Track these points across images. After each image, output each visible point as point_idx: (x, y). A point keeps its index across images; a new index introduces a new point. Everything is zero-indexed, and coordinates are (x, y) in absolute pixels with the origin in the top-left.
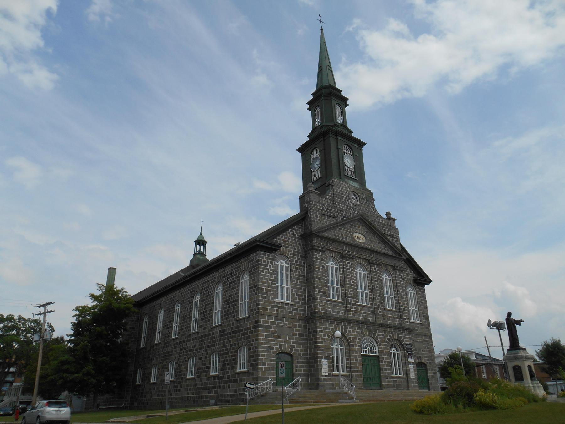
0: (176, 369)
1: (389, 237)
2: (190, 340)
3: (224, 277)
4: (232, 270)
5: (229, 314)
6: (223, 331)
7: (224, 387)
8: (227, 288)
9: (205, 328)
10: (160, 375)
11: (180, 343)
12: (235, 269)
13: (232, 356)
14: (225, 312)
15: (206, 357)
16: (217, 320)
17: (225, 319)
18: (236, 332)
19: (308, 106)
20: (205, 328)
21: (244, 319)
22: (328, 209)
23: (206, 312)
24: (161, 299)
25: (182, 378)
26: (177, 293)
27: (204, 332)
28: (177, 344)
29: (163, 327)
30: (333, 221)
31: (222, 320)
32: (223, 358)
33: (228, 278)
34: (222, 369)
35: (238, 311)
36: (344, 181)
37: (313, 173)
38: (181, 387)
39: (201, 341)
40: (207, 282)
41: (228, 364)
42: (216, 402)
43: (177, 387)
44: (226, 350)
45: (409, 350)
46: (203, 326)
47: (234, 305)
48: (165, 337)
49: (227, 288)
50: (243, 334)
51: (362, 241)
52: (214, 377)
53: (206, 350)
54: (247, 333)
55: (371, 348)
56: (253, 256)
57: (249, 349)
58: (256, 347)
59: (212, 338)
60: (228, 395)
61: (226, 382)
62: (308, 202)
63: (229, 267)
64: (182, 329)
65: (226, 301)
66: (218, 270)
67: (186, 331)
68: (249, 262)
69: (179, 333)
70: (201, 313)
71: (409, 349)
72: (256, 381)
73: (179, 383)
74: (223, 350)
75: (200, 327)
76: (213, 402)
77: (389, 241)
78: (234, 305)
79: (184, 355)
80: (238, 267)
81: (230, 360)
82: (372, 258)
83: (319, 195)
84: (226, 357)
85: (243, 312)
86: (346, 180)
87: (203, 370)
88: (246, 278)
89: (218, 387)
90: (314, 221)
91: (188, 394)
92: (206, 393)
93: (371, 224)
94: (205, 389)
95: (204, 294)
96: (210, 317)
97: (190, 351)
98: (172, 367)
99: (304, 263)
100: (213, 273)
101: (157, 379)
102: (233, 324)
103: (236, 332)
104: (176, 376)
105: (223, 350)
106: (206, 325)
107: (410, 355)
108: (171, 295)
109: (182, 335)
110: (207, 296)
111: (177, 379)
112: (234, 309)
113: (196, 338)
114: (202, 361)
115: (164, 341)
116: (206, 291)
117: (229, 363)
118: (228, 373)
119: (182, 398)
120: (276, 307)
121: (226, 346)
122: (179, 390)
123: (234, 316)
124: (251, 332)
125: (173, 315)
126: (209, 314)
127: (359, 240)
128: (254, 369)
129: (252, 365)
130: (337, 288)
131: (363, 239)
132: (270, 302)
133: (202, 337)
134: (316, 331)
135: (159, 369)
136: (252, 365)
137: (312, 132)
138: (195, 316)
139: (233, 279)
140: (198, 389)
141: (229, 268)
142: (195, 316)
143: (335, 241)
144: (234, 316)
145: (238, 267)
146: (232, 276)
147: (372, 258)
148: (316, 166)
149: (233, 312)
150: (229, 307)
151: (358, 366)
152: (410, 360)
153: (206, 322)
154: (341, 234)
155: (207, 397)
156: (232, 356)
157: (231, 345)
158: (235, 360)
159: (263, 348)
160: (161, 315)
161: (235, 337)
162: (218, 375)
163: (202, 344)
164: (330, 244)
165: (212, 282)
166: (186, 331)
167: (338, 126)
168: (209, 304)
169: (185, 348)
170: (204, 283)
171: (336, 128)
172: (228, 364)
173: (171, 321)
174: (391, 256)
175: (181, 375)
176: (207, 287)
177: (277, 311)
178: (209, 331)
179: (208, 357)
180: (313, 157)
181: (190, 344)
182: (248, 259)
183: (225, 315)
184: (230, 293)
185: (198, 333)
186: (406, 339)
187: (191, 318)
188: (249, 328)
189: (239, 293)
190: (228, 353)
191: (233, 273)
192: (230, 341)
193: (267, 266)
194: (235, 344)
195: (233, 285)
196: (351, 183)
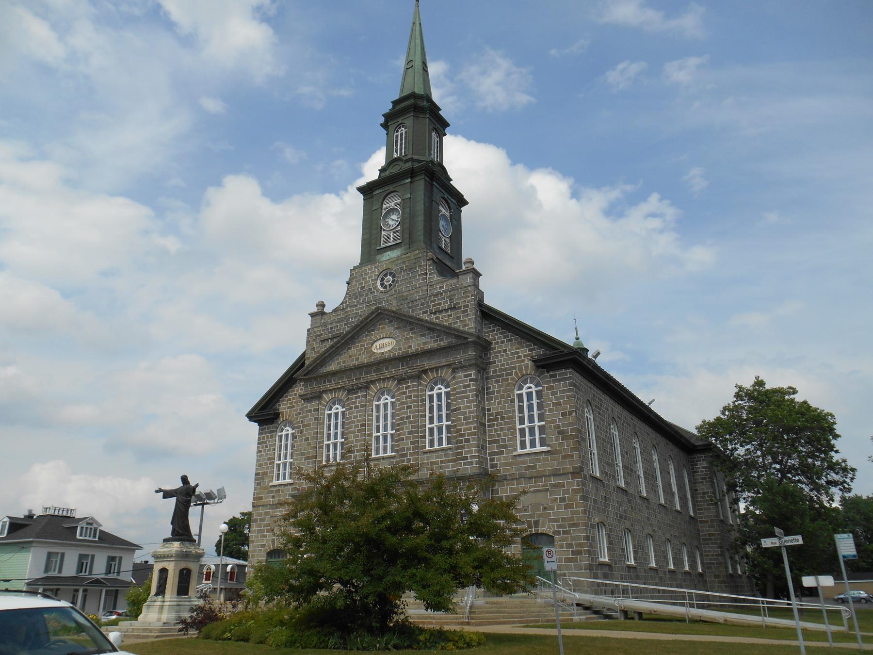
22: (332, 328)
86: (378, 257)
120: (272, 492)
127: (382, 351)
132: (266, 488)
143: (334, 374)
159: (254, 547)
164: (330, 381)
177: (273, 497)
193: (265, 442)
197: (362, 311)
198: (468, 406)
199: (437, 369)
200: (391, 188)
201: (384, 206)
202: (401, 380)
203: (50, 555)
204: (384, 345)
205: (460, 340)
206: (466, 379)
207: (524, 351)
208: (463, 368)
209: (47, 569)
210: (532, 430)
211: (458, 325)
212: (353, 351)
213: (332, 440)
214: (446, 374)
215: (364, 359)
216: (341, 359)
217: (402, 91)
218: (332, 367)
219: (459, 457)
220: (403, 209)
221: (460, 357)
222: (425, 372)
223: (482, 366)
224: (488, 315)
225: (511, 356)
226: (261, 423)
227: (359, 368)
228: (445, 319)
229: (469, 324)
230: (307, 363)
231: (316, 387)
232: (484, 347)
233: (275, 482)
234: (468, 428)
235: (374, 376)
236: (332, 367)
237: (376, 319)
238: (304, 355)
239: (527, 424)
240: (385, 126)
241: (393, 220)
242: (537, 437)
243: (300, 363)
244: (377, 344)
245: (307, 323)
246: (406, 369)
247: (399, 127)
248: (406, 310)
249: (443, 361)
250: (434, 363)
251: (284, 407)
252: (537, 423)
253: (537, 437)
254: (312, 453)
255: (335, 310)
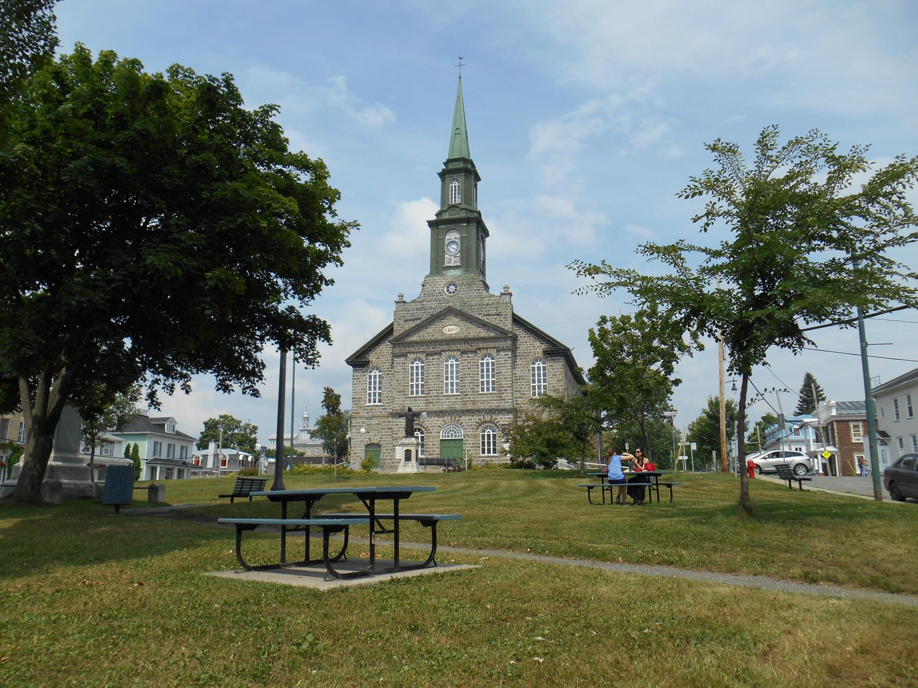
86: (444, 272)
143: (417, 343)
197: (435, 307)
198: (506, 371)
199: (487, 348)
200: (452, 226)
201: (447, 237)
202: (464, 352)
203: (156, 443)
204: (452, 329)
205: (503, 334)
206: (505, 356)
207: (537, 344)
208: (504, 350)
209: (154, 454)
210: (417, 386)
211: (501, 325)
212: (429, 330)
213: (415, 383)
214: (493, 352)
215: (438, 336)
216: (421, 334)
217: (452, 150)
218: (415, 338)
219: (500, 399)
220: (462, 243)
221: (501, 344)
222: (479, 349)
223: (514, 349)
224: (517, 320)
225: (529, 346)
226: (354, 366)
227: (436, 342)
228: (493, 320)
229: (508, 325)
230: (395, 334)
231: (404, 350)
232: (515, 339)
233: (368, 404)
234: (506, 383)
235: (445, 347)
236: (415, 338)
237: (449, 312)
238: (392, 324)
239: (536, 384)
240: (442, 175)
241: (453, 248)
242: (377, 398)
243: (389, 331)
244: (447, 328)
245: (394, 307)
246: (465, 346)
247: (454, 180)
248: (466, 310)
249: (492, 345)
250: (485, 345)
251: (372, 357)
252: (420, 382)
253: (377, 398)
254: (402, 388)
255: (414, 301)
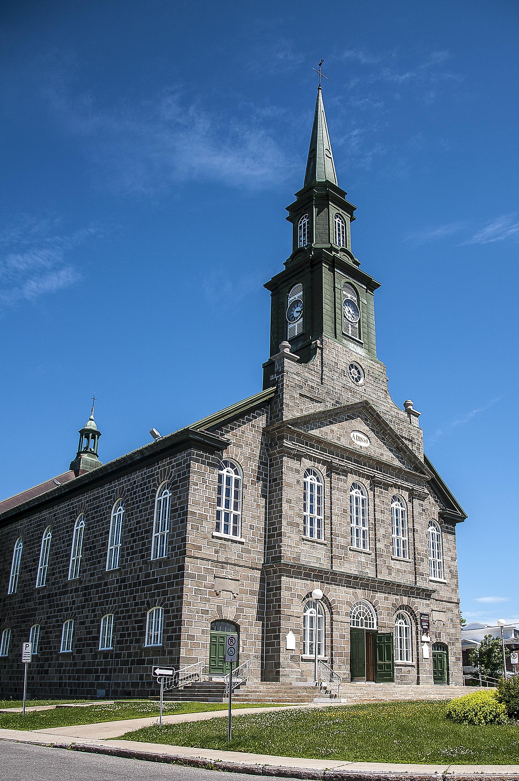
0: (42, 638)
1: (406, 442)
2: (66, 592)
3: (128, 490)
4: (143, 479)
5: (134, 553)
6: (123, 580)
7: (121, 671)
8: (132, 509)
9: (92, 575)
10: (14, 646)
11: (49, 596)
12: (148, 477)
13: (137, 622)
14: (127, 549)
15: (92, 622)
16: (112, 562)
17: (126, 560)
18: (145, 583)
19: (288, 214)
20: (92, 575)
21: (160, 563)
23: (95, 547)
24: (20, 522)
25: (51, 653)
26: (45, 514)
27: (90, 581)
28: (44, 597)
29: (21, 568)
30: (319, 408)
31: (121, 562)
32: (121, 623)
33: (135, 493)
34: (119, 642)
35: (149, 549)
36: (340, 342)
37: (290, 326)
38: (49, 667)
39: (84, 595)
40: (98, 498)
41: (129, 635)
42: (107, 694)
43: (42, 666)
44: (127, 611)
45: (423, 624)
46: (90, 570)
47: (143, 538)
48: (25, 586)
49: (132, 509)
50: (156, 588)
51: (364, 444)
52: (106, 654)
53: (94, 611)
54: (163, 586)
55: (366, 619)
56: (180, 457)
57: (166, 612)
58: (180, 610)
59: (103, 591)
60: (128, 683)
61: (126, 663)
62: (278, 373)
63: (138, 473)
64: (54, 574)
65: (130, 531)
66: (118, 478)
67: (60, 577)
68: (173, 467)
69: (47, 580)
70: (86, 550)
71: (425, 621)
72: (175, 662)
73: (47, 660)
74: (122, 612)
75: (85, 571)
76: (102, 692)
77: (407, 447)
78: (143, 538)
79: (56, 616)
80: (153, 475)
81: (134, 628)
82: (379, 476)
83: (299, 362)
84: (126, 623)
85: (157, 549)
86: (345, 341)
87: (87, 639)
88: (120, 510)
89: (111, 669)
90: (288, 405)
91: (61, 678)
92: (91, 678)
93: (380, 417)
94: (89, 671)
95: (93, 518)
96: (101, 556)
97: (67, 610)
98: (35, 632)
99: (266, 475)
100: (110, 482)
101: (10, 651)
102: (141, 570)
103: (145, 583)
104: (41, 649)
105: (122, 612)
106: (95, 569)
107: (426, 631)
108: (37, 516)
109: (54, 584)
110: (98, 521)
111: (43, 654)
112: (144, 544)
113: (77, 590)
114: (86, 628)
115: (23, 591)
116: (96, 512)
117: (131, 630)
118: (128, 648)
119: (51, 684)
121: (126, 606)
122: (47, 672)
123: (143, 557)
124: (171, 585)
125: (39, 550)
126: (100, 551)
127: (358, 443)
128: (173, 645)
129: (170, 638)
130: (319, 521)
131: (365, 441)
133: (86, 588)
134: (280, 588)
135: (13, 636)
136: (170, 638)
137: (293, 257)
138: (76, 555)
139: (144, 495)
140: (78, 671)
141: (137, 476)
142: (76, 555)
144: (143, 557)
145: (153, 475)
146: (143, 490)
147: (379, 476)
148: (296, 315)
149: (141, 551)
150: (135, 541)
151: (344, 645)
152: (425, 638)
153: (94, 564)
154: (330, 433)
155: (92, 685)
156: (137, 622)
157: (136, 604)
158: (142, 628)
160: (18, 547)
161: (143, 590)
162: (113, 651)
163: (86, 600)
165: (107, 499)
166: (60, 577)
167: (337, 251)
168: (101, 535)
169: (58, 606)
170: (94, 499)
171: (333, 253)
172: (129, 635)
173: (36, 560)
174: (398, 472)
175: (50, 648)
176: (98, 507)
178: (100, 579)
179: (96, 623)
180: (291, 299)
181: (67, 599)
182: (171, 463)
183: (128, 554)
184: (137, 518)
185: (80, 581)
186: (421, 606)
187: (69, 556)
188: (168, 578)
189: (152, 518)
190: (130, 617)
191: (145, 484)
192: (134, 599)
194: (143, 603)
195: (143, 505)
196: (352, 346)
